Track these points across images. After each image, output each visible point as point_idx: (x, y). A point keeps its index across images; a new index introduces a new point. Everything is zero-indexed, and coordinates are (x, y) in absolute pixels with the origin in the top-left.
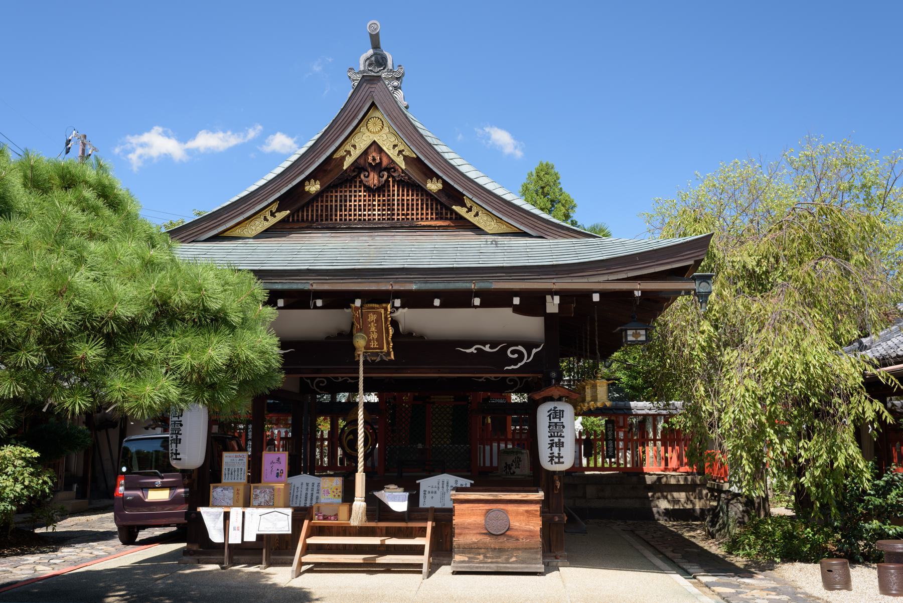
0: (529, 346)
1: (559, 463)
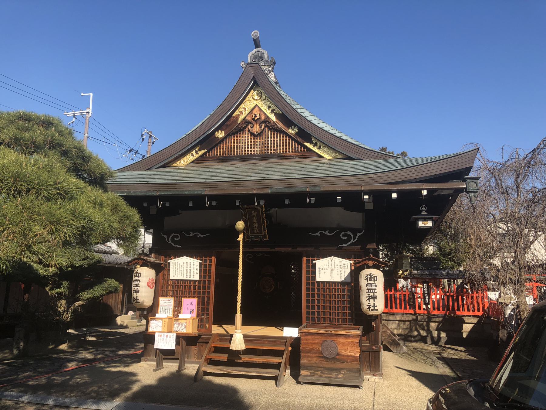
0: (355, 231)
1: (374, 310)
